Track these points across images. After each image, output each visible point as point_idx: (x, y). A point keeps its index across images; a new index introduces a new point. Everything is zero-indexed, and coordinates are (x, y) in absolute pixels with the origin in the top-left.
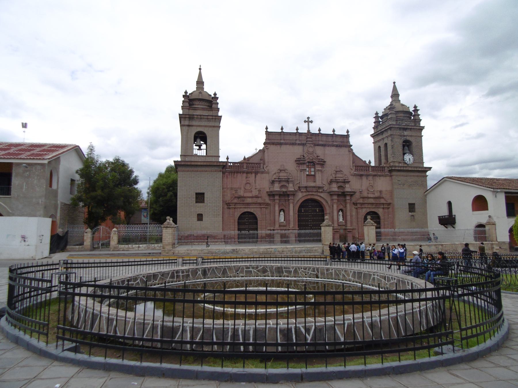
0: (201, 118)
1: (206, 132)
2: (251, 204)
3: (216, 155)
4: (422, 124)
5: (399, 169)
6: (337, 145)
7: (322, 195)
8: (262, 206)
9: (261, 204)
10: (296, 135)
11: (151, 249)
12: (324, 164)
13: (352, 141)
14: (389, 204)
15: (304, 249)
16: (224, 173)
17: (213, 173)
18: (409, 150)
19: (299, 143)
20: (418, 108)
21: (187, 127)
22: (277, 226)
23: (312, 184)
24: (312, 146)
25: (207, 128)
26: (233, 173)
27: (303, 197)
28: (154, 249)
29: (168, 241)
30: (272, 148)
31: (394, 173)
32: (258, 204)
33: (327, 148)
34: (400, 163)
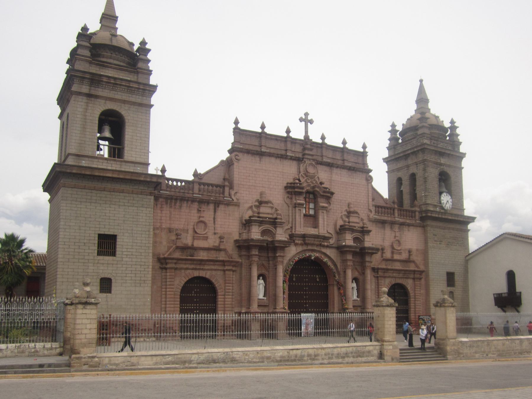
0: (114, 83)
1: (123, 112)
2: (207, 263)
3: (142, 161)
4: (462, 149)
6: (350, 167)
7: (328, 252)
8: (226, 268)
9: (226, 264)
11: (27, 354)
14: (421, 272)
15: (351, 349)
16: (156, 199)
17: (134, 195)
18: (447, 189)
19: (292, 157)
21: (85, 98)
22: (255, 307)
23: (312, 231)
24: (314, 163)
25: (127, 105)
26: (173, 201)
27: (298, 253)
28: (35, 354)
29: (88, 336)
31: (429, 222)
32: (220, 263)
33: (335, 170)
34: (435, 206)
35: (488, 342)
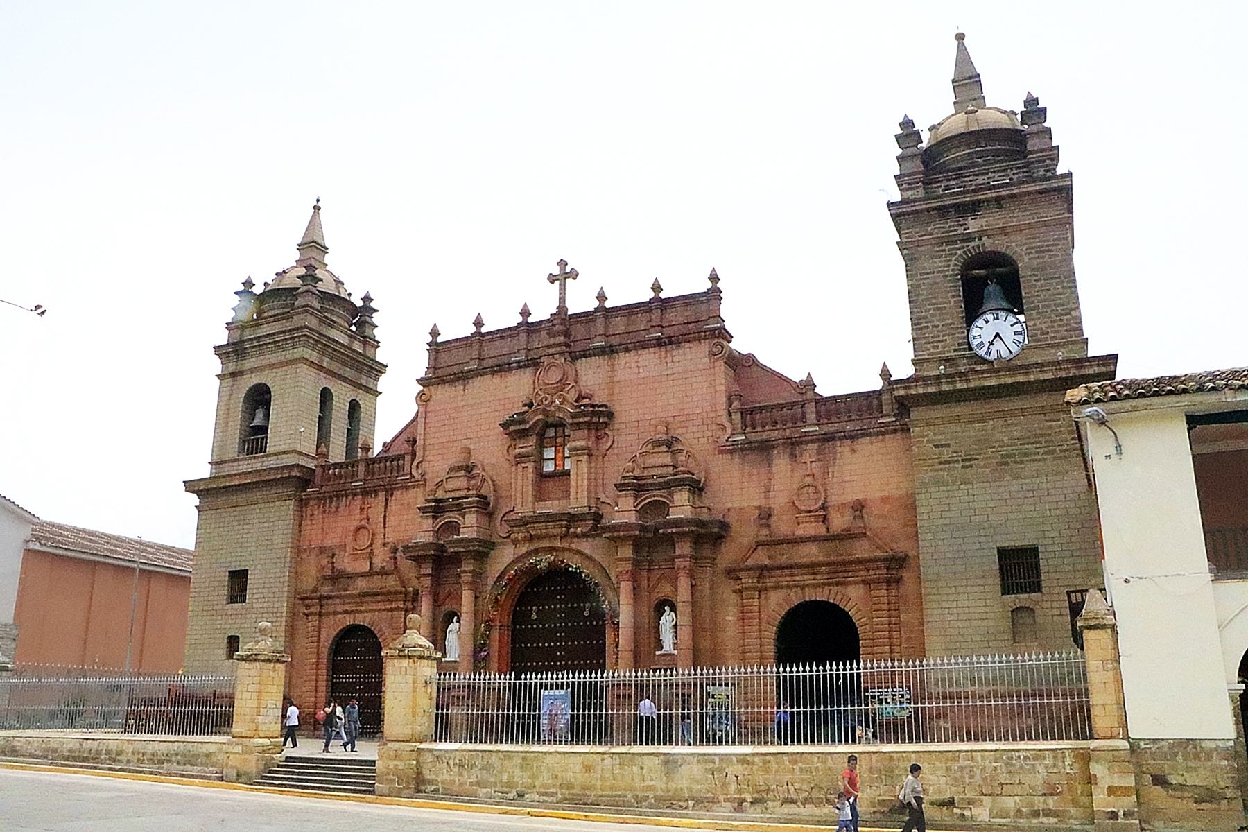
5: (931, 389)
10: (518, 335)
12: (606, 425)
13: (731, 314)
16: (302, 503)
20: (373, 305)
30: (442, 394)
33: (623, 359)
35: (524, 759)
